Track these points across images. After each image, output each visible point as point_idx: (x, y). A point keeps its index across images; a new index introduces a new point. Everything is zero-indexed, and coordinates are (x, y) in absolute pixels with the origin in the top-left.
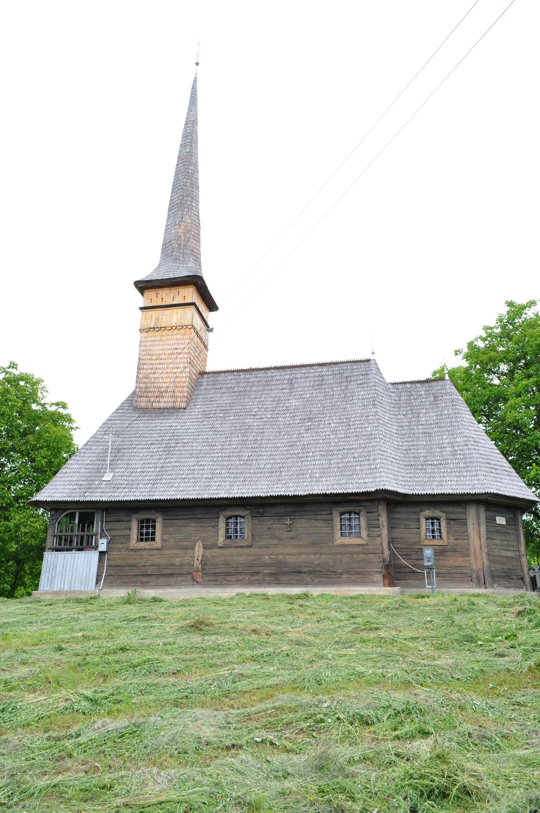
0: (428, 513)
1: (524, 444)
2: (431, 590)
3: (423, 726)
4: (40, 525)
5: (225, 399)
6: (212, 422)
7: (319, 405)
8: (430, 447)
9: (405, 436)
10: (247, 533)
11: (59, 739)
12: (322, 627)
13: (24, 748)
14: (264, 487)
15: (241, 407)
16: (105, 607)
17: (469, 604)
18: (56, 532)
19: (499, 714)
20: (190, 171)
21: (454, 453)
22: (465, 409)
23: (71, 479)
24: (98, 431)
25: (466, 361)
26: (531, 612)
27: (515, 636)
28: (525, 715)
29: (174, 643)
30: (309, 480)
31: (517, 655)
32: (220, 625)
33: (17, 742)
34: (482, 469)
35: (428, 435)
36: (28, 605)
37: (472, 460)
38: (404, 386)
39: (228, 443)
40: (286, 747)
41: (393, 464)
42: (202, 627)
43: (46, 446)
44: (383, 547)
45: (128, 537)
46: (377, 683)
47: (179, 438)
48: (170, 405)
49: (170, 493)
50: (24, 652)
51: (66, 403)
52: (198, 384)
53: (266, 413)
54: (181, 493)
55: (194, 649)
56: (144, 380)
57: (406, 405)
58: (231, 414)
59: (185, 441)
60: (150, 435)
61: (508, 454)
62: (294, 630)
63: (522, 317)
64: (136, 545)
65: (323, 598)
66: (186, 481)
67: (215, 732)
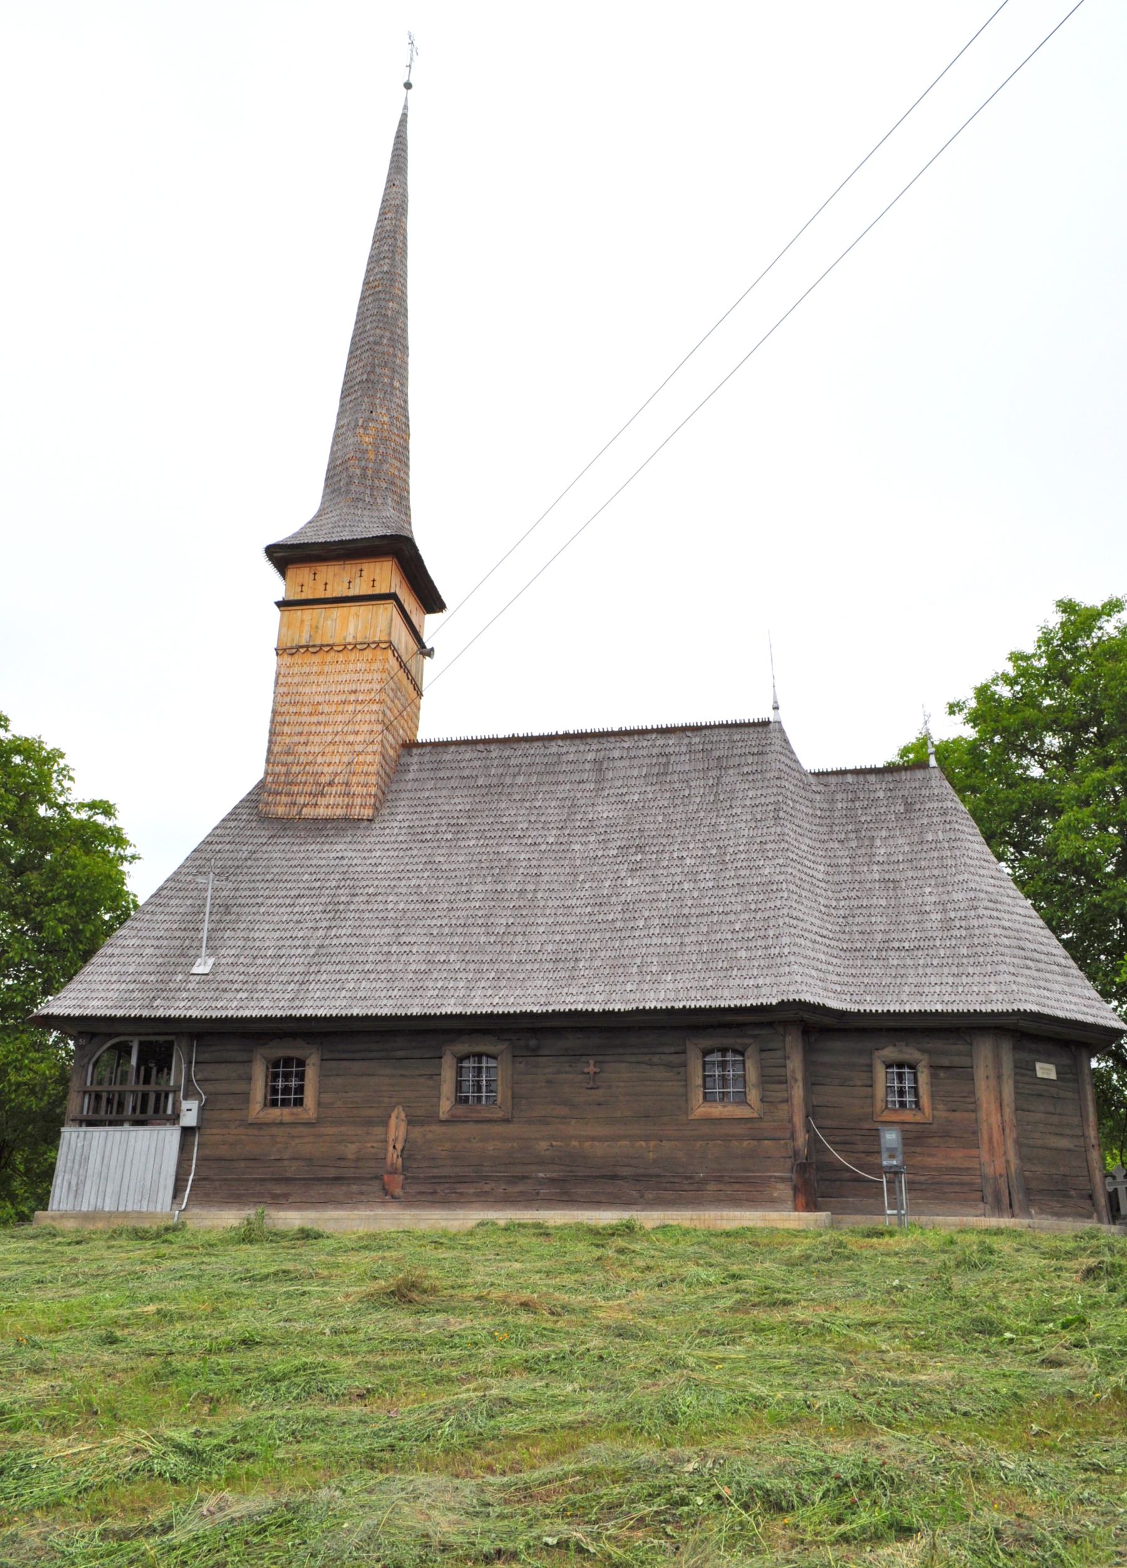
0: (890, 1052)
1: (1096, 906)
2: (895, 1219)
3: (899, 1514)
4: (50, 1069)
5: (457, 800)
6: (430, 851)
7: (660, 818)
8: (896, 911)
9: (844, 886)
10: (502, 1092)
11: (124, 1536)
12: (669, 1298)
13: (53, 1554)
14: (541, 991)
15: (492, 819)
16: (197, 1248)
17: (982, 1252)
18: (89, 1083)
19: (1056, 1489)
20: (389, 313)
21: (947, 925)
22: (971, 831)
23: (124, 969)
24: (182, 866)
25: (973, 727)
26: (1114, 1270)
27: (1083, 1321)
28: (1112, 1492)
29: (355, 1331)
30: (637, 979)
31: (1089, 1361)
32: (453, 1292)
33: (37, 1542)
34: (1008, 959)
35: (891, 885)
36: (31, 1243)
37: (986, 940)
38: (840, 779)
39: (464, 897)
40: (610, 1557)
41: (817, 946)
42: (414, 1295)
43: (67, 897)
44: (794, 1126)
45: (245, 1097)
46: (796, 1420)
47: (357, 883)
48: (339, 812)
49: (338, 1004)
50: (35, 1345)
51: (111, 803)
52: (399, 768)
53: (545, 832)
54: (361, 1003)
55: (400, 1343)
56: (284, 758)
57: (844, 821)
58: (470, 835)
59: (371, 890)
60: (293, 878)
61: (1059, 927)
62: (610, 1303)
63: (1093, 634)
64: (262, 1114)
65: (665, 1234)
66: (372, 976)
67: (458, 1523)
